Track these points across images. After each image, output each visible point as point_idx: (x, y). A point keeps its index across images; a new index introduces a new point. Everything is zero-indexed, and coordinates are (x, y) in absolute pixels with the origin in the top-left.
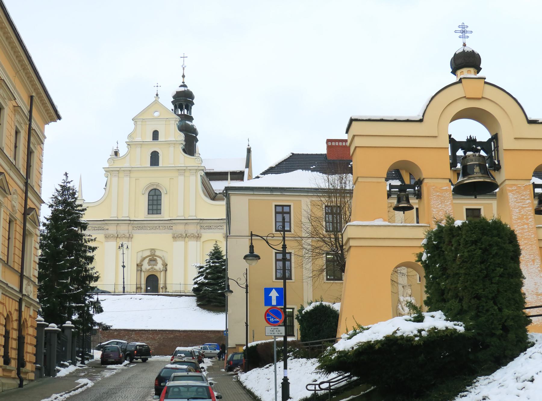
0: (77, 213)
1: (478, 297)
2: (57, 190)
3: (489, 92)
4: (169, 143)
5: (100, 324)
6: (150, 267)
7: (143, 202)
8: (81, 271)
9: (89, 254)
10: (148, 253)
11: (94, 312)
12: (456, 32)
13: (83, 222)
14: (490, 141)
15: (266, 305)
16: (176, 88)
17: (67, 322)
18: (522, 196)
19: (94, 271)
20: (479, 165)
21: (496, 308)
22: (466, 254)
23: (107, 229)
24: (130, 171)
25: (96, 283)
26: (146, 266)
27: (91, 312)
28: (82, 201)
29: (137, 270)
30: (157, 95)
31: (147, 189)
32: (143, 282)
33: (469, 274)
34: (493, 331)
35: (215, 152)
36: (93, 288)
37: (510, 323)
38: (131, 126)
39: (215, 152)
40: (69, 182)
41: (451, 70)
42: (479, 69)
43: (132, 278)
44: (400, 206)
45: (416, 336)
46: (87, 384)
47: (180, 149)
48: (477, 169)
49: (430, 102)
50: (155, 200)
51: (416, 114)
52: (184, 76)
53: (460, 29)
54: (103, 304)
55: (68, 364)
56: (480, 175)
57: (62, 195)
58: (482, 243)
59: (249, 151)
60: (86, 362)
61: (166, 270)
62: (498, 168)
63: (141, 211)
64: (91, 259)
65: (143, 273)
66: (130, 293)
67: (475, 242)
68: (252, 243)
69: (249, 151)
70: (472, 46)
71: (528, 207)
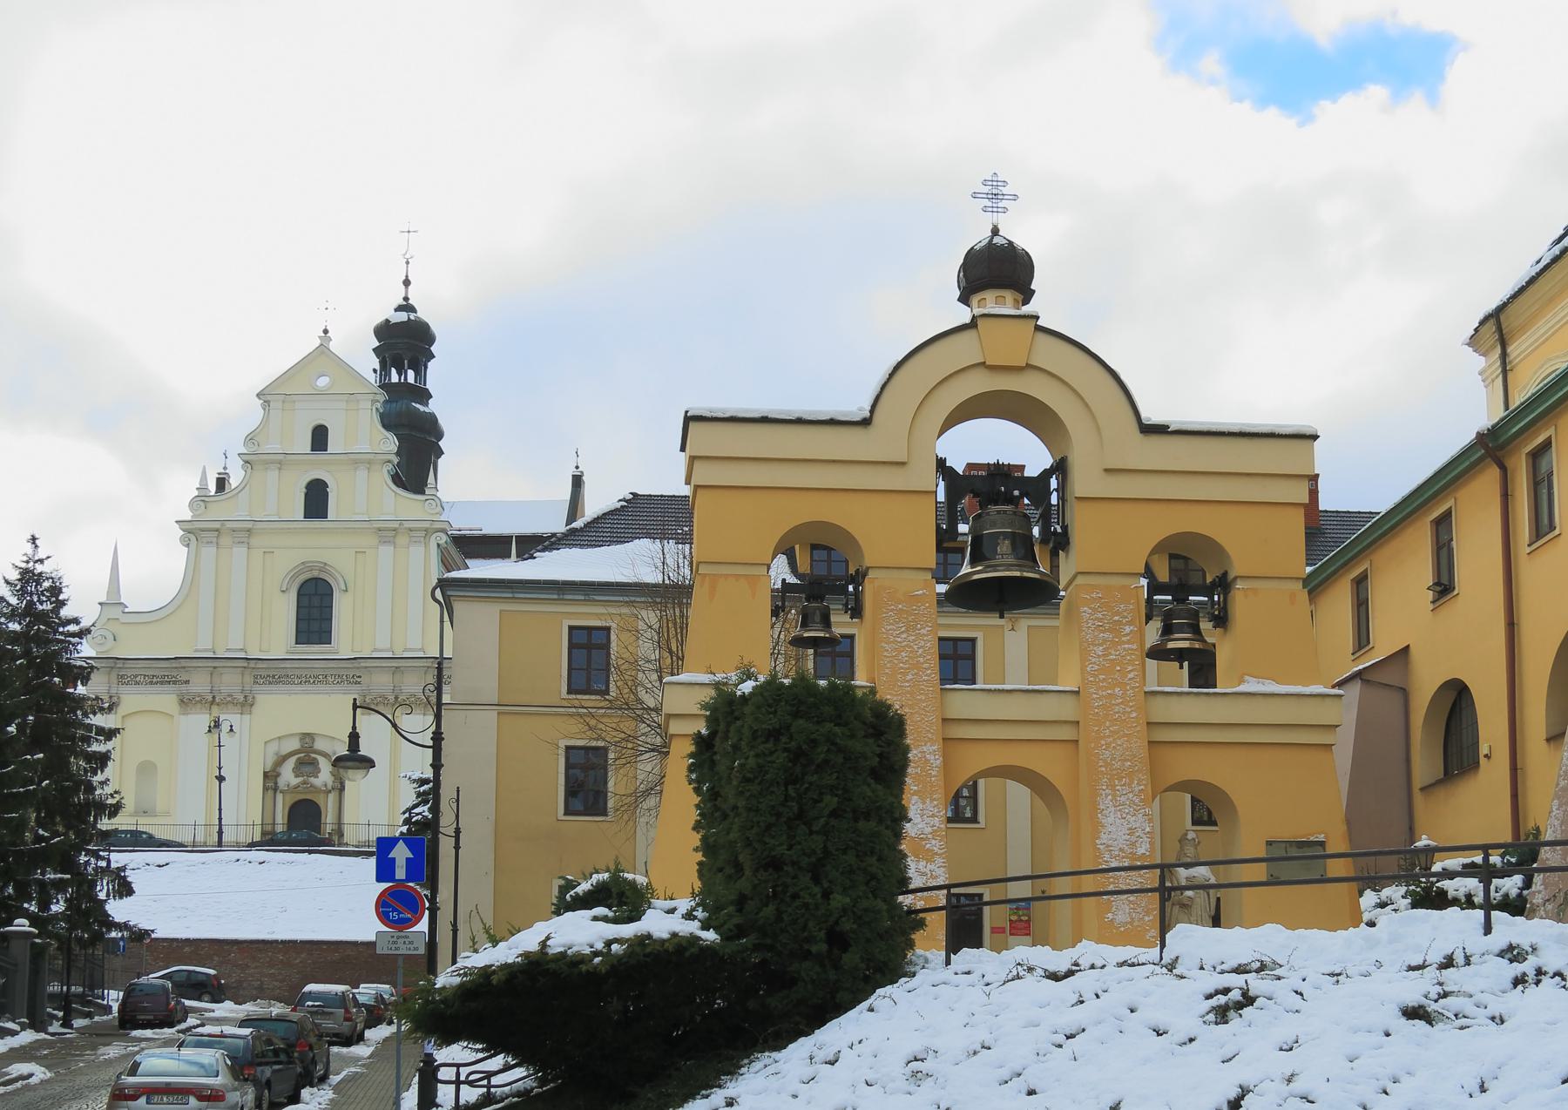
0: (62, 641)
1: (775, 864)
2: (7, 582)
3: (1046, 354)
4: (356, 461)
5: (124, 926)
6: (300, 779)
7: (285, 611)
8: (76, 791)
9: (95, 747)
10: (294, 744)
11: (108, 895)
12: (975, 195)
13: (79, 663)
14: (1046, 474)
15: (380, 879)
16: (386, 311)
17: (17, 921)
18: (1118, 613)
19: (108, 790)
20: (1013, 537)
21: (816, 890)
22: (752, 762)
23: (187, 682)
24: (249, 530)
25: (114, 820)
26: (288, 776)
27: (102, 896)
28: (120, 608)
29: (265, 789)
30: (326, 331)
31: (293, 578)
32: (281, 819)
33: (757, 810)
34: (806, 947)
35: (481, 481)
36: (105, 835)
37: (847, 925)
38: (256, 413)
39: (481, 481)
40: (41, 561)
41: (958, 293)
42: (1027, 295)
43: (246, 807)
44: (1171, 645)
45: (596, 954)
46: (31, 1075)
47: (383, 476)
48: (1004, 547)
49: (891, 375)
50: (314, 607)
51: (855, 404)
52: (407, 283)
53: (986, 189)
54: (131, 876)
55: (17, 1028)
56: (1011, 560)
57: (22, 593)
58: (791, 738)
59: (577, 482)
60: (79, 1023)
61: (342, 789)
62: (1059, 543)
63: (276, 633)
64: (103, 760)
65: (280, 797)
66: (238, 846)
67: (774, 735)
68: (354, 727)
69: (577, 482)
70: (1019, 233)
71: (1128, 642)
